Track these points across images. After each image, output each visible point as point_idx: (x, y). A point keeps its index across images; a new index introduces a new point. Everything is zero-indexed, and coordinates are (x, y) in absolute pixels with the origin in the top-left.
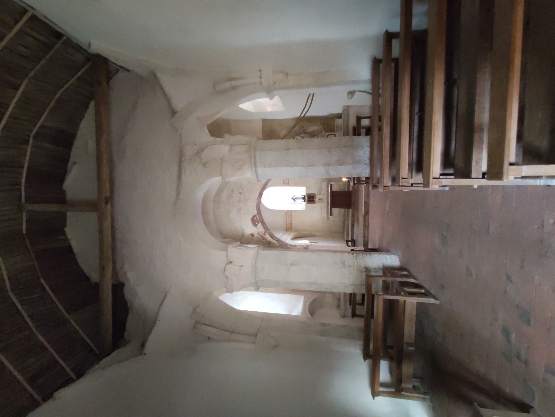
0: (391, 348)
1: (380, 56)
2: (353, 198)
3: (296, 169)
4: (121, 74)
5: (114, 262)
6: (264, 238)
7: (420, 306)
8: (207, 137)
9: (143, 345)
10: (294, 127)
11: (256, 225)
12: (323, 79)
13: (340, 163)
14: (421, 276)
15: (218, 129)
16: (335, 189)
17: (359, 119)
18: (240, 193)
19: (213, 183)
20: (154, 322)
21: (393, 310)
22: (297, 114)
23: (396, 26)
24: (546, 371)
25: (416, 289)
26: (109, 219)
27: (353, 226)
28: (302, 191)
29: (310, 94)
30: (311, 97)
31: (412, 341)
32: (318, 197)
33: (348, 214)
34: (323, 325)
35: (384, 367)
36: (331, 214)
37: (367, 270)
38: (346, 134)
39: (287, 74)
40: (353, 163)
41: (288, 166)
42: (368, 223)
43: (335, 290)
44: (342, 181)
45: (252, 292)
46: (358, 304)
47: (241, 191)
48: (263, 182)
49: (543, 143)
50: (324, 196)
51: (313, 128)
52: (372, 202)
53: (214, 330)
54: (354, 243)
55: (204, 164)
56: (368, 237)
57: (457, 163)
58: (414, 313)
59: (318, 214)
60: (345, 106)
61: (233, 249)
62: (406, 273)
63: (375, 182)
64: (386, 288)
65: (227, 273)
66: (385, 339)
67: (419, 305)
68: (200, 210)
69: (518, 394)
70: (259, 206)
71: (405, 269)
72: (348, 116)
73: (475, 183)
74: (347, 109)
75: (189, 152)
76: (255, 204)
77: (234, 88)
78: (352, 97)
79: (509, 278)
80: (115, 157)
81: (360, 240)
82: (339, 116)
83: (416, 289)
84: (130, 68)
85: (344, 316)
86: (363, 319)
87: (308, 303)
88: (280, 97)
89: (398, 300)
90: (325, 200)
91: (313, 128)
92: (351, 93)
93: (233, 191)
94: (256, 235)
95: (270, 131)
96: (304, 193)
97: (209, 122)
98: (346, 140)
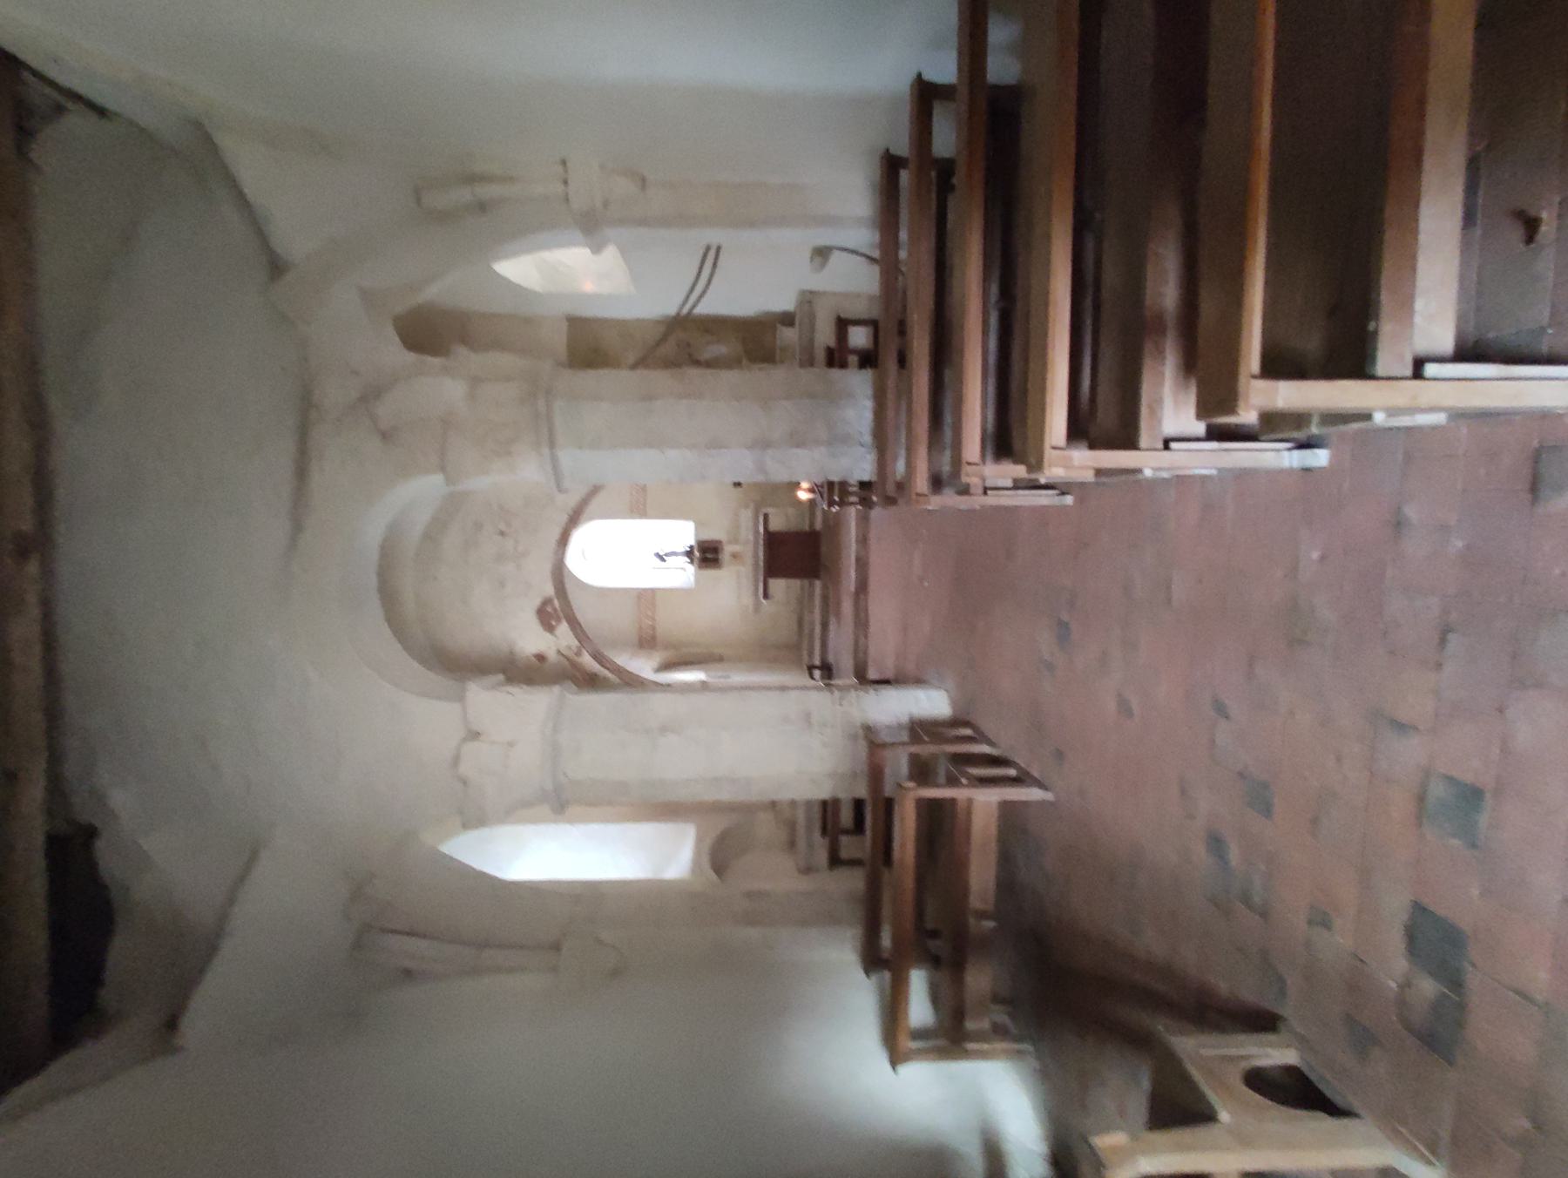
0: (934, 934)
1: (902, 146)
2: (824, 549)
3: (673, 454)
4: (76, 122)
5: (55, 758)
6: (574, 665)
7: (1008, 810)
8: (394, 354)
9: (172, 1024)
10: (658, 344)
11: (550, 628)
12: (748, 207)
13: (797, 440)
14: (1005, 737)
15: (429, 333)
16: (777, 524)
17: (842, 325)
18: (502, 533)
19: (417, 494)
20: (209, 946)
21: (939, 823)
22: (671, 310)
23: (944, 69)
24: (1310, 922)
25: (994, 767)
26: (35, 612)
27: (825, 625)
28: (683, 534)
29: (708, 249)
30: (712, 256)
31: (989, 906)
32: (728, 550)
33: (811, 595)
34: (749, 895)
35: (918, 982)
36: (766, 596)
37: (869, 731)
38: (809, 362)
39: (644, 180)
40: (829, 441)
41: (649, 444)
42: (867, 615)
43: (785, 795)
44: (800, 502)
45: (542, 828)
46: (849, 828)
47: (502, 527)
48: (572, 500)
49: (1312, 344)
50: (745, 547)
51: (720, 349)
52: (875, 560)
53: (421, 945)
54: (828, 670)
55: (386, 436)
56: (865, 653)
57: (1107, 419)
58: (993, 830)
59: (730, 599)
60: (803, 293)
62: (968, 732)
63: (891, 489)
64: (922, 771)
65: (464, 769)
66: (920, 913)
67: (1007, 808)
68: (373, 581)
69: (1249, 991)
70: (559, 573)
71: (966, 724)
72: (812, 318)
73: (1147, 461)
74: (808, 299)
75: (334, 393)
76: (547, 567)
77: (482, 207)
78: (823, 265)
79: (1221, 710)
80: (55, 402)
81: (844, 661)
82: (787, 319)
83: (994, 767)
84: (109, 103)
85: (807, 870)
87: (708, 842)
88: (624, 252)
89: (953, 801)
90: (749, 560)
91: (720, 349)
92: (822, 254)
93: (478, 526)
95: (589, 346)
97: (399, 309)
98: (807, 376)
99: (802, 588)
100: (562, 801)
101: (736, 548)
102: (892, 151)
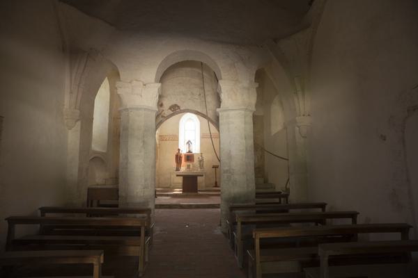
7: (92, 265)
11: (170, 108)
28: (196, 149)
32: (191, 164)
50: (195, 168)
56: (220, 178)
61: (156, 90)
86: (182, 177)
96: (194, 152)
99: (179, 183)
100: (86, 119)
101: (191, 167)
102: (358, 215)
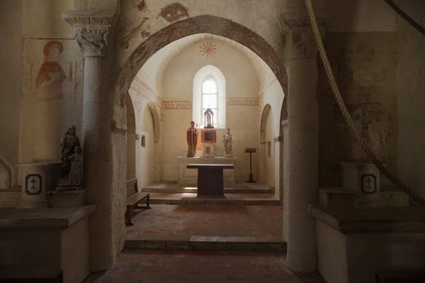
11: (164, 13)
94: (142, 14)
